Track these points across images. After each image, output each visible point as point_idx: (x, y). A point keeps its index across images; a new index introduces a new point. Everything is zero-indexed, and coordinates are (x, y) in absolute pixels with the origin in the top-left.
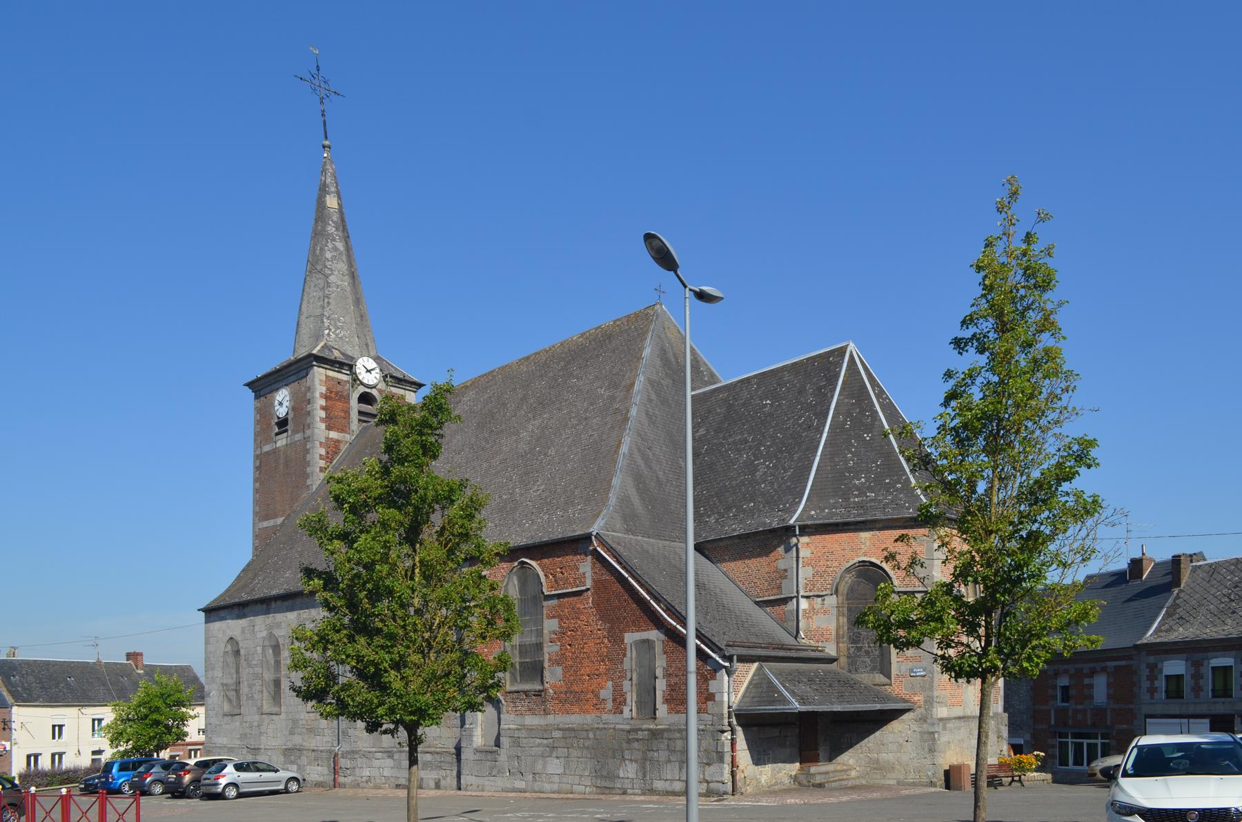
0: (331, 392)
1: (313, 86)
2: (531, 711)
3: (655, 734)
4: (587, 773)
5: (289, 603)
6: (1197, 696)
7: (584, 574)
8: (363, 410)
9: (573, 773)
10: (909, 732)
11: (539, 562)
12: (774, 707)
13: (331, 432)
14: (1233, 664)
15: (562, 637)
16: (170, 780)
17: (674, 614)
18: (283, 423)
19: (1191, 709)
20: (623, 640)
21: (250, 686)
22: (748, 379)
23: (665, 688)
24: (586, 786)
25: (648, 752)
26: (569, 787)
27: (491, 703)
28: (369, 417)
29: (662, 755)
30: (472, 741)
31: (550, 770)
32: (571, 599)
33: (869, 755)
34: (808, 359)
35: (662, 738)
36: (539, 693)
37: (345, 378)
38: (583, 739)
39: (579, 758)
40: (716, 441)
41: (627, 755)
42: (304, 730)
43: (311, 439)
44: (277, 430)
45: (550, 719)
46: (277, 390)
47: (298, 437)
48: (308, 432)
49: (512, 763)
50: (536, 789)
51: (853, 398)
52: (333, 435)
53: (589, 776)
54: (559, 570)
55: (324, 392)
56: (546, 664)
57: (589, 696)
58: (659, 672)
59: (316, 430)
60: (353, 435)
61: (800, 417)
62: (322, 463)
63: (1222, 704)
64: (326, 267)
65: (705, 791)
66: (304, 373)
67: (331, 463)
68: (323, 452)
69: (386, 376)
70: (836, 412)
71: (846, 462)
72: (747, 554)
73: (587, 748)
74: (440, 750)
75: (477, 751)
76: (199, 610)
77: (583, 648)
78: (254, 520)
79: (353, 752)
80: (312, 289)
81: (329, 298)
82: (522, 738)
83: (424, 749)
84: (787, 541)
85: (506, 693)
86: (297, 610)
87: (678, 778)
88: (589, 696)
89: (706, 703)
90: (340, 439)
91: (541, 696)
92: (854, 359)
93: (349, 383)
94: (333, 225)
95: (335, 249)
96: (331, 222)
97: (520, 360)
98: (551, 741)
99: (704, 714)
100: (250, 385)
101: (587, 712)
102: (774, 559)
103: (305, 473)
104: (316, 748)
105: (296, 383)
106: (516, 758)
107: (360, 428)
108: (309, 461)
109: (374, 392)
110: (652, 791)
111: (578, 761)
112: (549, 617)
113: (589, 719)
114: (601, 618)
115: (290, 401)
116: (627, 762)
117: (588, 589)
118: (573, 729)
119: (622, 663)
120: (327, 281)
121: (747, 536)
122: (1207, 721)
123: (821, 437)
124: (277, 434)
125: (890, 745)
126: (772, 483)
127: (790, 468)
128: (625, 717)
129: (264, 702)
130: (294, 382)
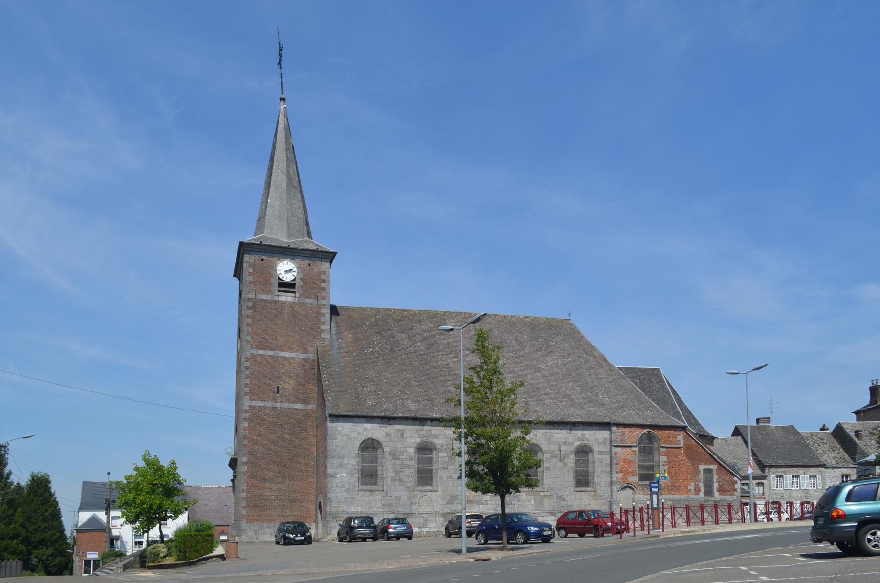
58: (715, 480)
100: (335, 253)
112: (662, 455)
113: (683, 497)
115: (298, 273)
117: (682, 447)
118: (678, 501)
119: (698, 476)
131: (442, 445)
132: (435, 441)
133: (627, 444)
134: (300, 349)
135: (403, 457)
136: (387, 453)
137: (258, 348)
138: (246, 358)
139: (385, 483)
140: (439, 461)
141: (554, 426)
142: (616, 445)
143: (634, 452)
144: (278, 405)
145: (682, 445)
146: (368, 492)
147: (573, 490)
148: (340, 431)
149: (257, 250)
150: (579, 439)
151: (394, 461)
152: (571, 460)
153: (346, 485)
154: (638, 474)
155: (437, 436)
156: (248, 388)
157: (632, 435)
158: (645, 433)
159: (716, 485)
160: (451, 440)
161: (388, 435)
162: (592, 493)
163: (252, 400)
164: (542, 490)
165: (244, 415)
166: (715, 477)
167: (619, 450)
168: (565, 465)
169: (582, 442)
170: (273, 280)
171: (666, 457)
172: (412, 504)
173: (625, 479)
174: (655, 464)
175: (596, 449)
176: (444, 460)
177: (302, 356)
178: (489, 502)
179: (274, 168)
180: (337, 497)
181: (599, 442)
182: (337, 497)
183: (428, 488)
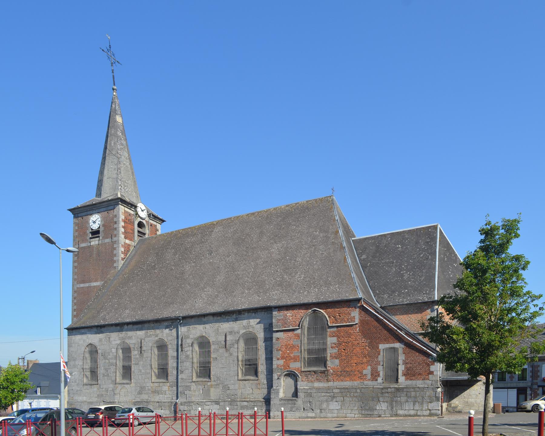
0: (126, 219)
1: (108, 56)
2: (318, 380)
3: (398, 390)
4: (356, 408)
5: (140, 326)
6: (512, 380)
7: (354, 317)
8: (139, 230)
9: (346, 408)
10: (480, 390)
11: (325, 310)
12: (462, 377)
13: (126, 240)
14: (527, 368)
15: (339, 346)
16: (89, 417)
17: (410, 336)
18: (95, 233)
19: (509, 385)
20: (378, 347)
21: (106, 370)
22: (385, 235)
23: (404, 369)
24: (355, 414)
25: (394, 398)
26: (344, 415)
27: (290, 377)
28: (142, 235)
29: (403, 399)
30: (278, 395)
31: (331, 407)
32: (346, 328)
33: (464, 400)
34: (417, 229)
35: (403, 391)
36: (324, 372)
37: (132, 212)
38: (354, 393)
39: (351, 401)
40: (374, 261)
41: (381, 399)
42: (150, 392)
43: (117, 242)
44: (91, 236)
45: (331, 384)
46: (91, 214)
47: (107, 240)
48: (115, 239)
49: (306, 405)
50: (322, 416)
51: (445, 248)
52: (127, 241)
53: (357, 409)
54: (337, 314)
55: (124, 219)
56: (328, 358)
57: (356, 373)
58: (400, 362)
59: (120, 238)
60: (135, 243)
61: (420, 254)
62: (122, 256)
63: (522, 383)
64: (118, 153)
65: (428, 414)
66: (112, 207)
67: (126, 256)
68: (123, 250)
69: (150, 214)
70: (439, 253)
71: (449, 275)
72: (409, 312)
73: (356, 397)
74: (253, 400)
75: (281, 400)
76: (65, 329)
77: (353, 351)
78: (73, 283)
79: (189, 402)
80: (110, 163)
81: (120, 170)
82: (313, 393)
83: (241, 400)
84: (432, 308)
85: (301, 372)
86: (144, 330)
87: (412, 409)
88: (356, 373)
89: (428, 375)
90: (130, 244)
91: (324, 373)
92: (442, 231)
93: (134, 216)
94: (120, 131)
95: (122, 144)
96: (119, 130)
97: (248, 215)
98: (332, 394)
99: (427, 380)
101: (355, 380)
102: (424, 315)
103: (113, 260)
104: (160, 401)
105: (106, 212)
106: (309, 402)
107: (138, 240)
108: (116, 254)
109: (144, 222)
110: (397, 415)
111: (350, 403)
112: (330, 336)
113: (356, 383)
114: (364, 337)
115: (101, 221)
116: (381, 403)
117: (357, 324)
118: (347, 388)
119: (377, 357)
120: (119, 161)
121: (411, 304)
122: (516, 390)
123: (435, 263)
124: (91, 238)
125: (473, 395)
126: (414, 282)
127: (422, 275)
128: (378, 382)
129: (117, 378)
130: (104, 211)
131: (135, 344)
133: (289, 327)
135: (110, 357)
142: (277, 329)
149: (79, 212)
159: (401, 368)
161: (101, 340)
166: (401, 358)
168: (231, 354)
169: (247, 330)
171: (336, 338)
179: (108, 141)
180: (72, 390)
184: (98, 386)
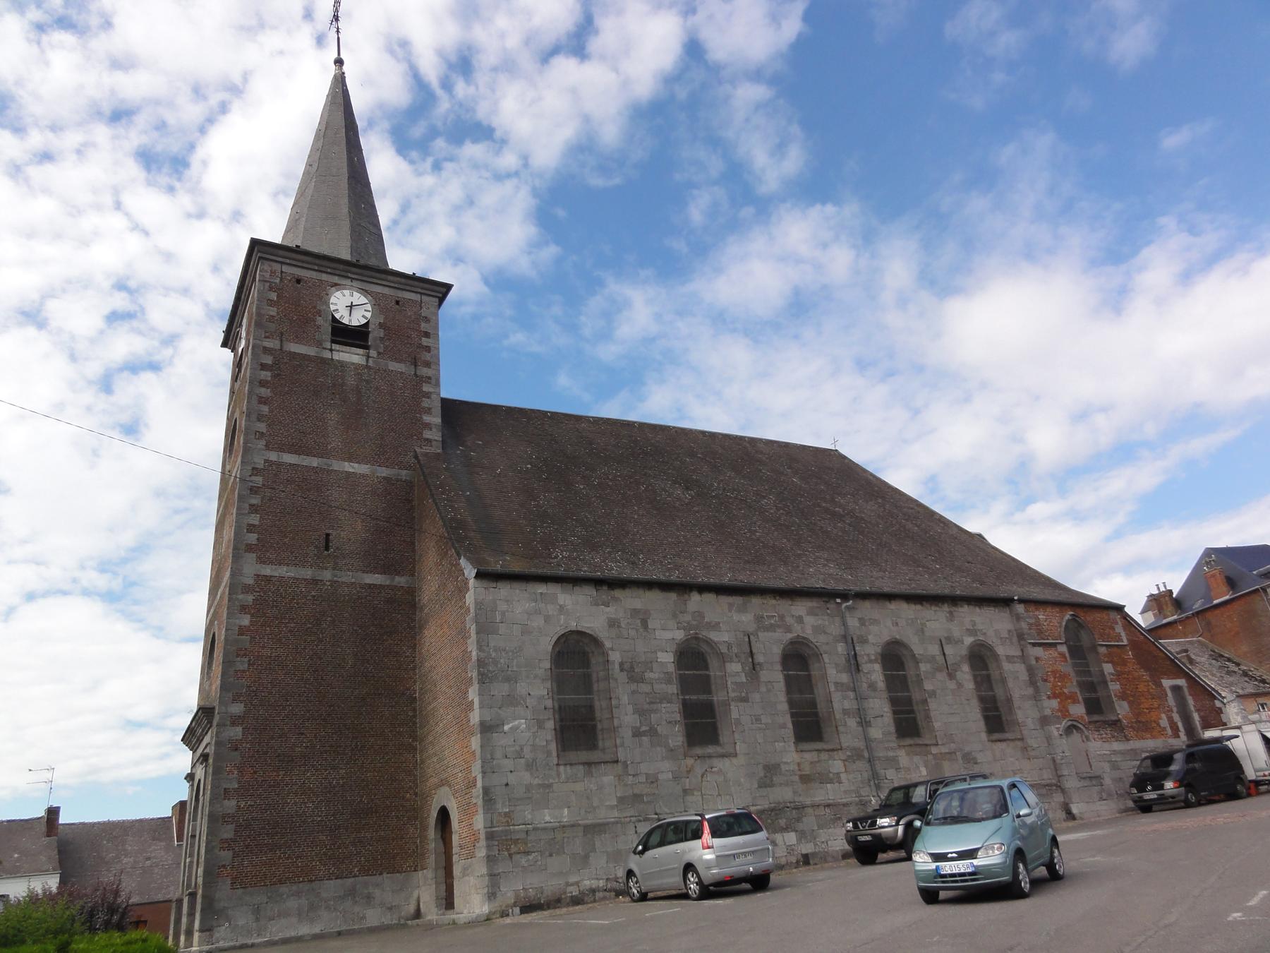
131: (729, 646)
132: (714, 636)
133: (1048, 639)
134: (378, 457)
135: (652, 675)
136: (617, 666)
137: (281, 449)
138: (253, 469)
139: (618, 741)
140: (729, 683)
141: (922, 604)
143: (1062, 655)
144: (327, 575)
145: (1125, 642)
146: (581, 767)
147: (986, 739)
148: (503, 613)
149: (288, 261)
150: (972, 632)
151: (634, 686)
152: (965, 674)
153: (527, 750)
154: (1080, 699)
155: (715, 626)
156: (256, 536)
157: (1050, 622)
158: (1069, 620)
160: (744, 635)
161: (613, 623)
162: (1019, 743)
163: (264, 563)
164: (934, 742)
165: (241, 597)
167: (1039, 651)
168: (960, 685)
170: (320, 320)
172: (685, 792)
173: (1064, 712)
174: (1095, 680)
175: (1001, 651)
176: (738, 680)
177: (384, 472)
178: (843, 776)
180: (507, 785)
181: (1001, 638)
182: (507, 785)
183: (710, 750)
184: (619, 767)
